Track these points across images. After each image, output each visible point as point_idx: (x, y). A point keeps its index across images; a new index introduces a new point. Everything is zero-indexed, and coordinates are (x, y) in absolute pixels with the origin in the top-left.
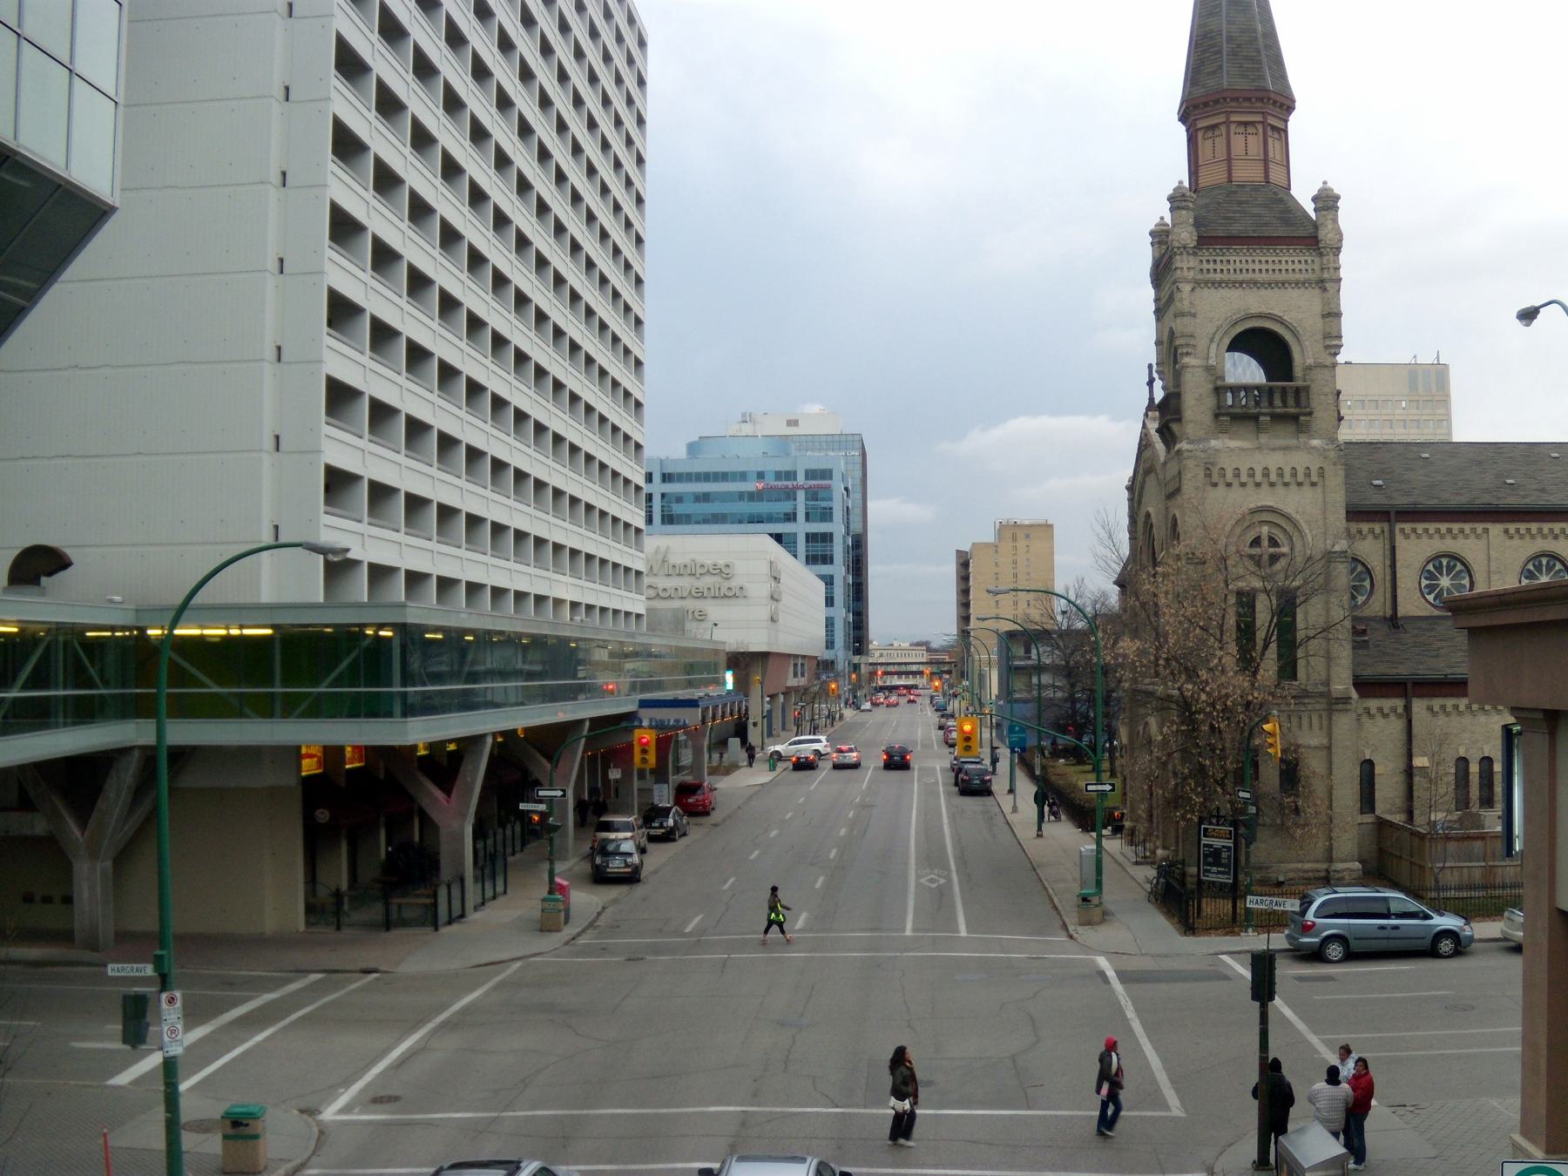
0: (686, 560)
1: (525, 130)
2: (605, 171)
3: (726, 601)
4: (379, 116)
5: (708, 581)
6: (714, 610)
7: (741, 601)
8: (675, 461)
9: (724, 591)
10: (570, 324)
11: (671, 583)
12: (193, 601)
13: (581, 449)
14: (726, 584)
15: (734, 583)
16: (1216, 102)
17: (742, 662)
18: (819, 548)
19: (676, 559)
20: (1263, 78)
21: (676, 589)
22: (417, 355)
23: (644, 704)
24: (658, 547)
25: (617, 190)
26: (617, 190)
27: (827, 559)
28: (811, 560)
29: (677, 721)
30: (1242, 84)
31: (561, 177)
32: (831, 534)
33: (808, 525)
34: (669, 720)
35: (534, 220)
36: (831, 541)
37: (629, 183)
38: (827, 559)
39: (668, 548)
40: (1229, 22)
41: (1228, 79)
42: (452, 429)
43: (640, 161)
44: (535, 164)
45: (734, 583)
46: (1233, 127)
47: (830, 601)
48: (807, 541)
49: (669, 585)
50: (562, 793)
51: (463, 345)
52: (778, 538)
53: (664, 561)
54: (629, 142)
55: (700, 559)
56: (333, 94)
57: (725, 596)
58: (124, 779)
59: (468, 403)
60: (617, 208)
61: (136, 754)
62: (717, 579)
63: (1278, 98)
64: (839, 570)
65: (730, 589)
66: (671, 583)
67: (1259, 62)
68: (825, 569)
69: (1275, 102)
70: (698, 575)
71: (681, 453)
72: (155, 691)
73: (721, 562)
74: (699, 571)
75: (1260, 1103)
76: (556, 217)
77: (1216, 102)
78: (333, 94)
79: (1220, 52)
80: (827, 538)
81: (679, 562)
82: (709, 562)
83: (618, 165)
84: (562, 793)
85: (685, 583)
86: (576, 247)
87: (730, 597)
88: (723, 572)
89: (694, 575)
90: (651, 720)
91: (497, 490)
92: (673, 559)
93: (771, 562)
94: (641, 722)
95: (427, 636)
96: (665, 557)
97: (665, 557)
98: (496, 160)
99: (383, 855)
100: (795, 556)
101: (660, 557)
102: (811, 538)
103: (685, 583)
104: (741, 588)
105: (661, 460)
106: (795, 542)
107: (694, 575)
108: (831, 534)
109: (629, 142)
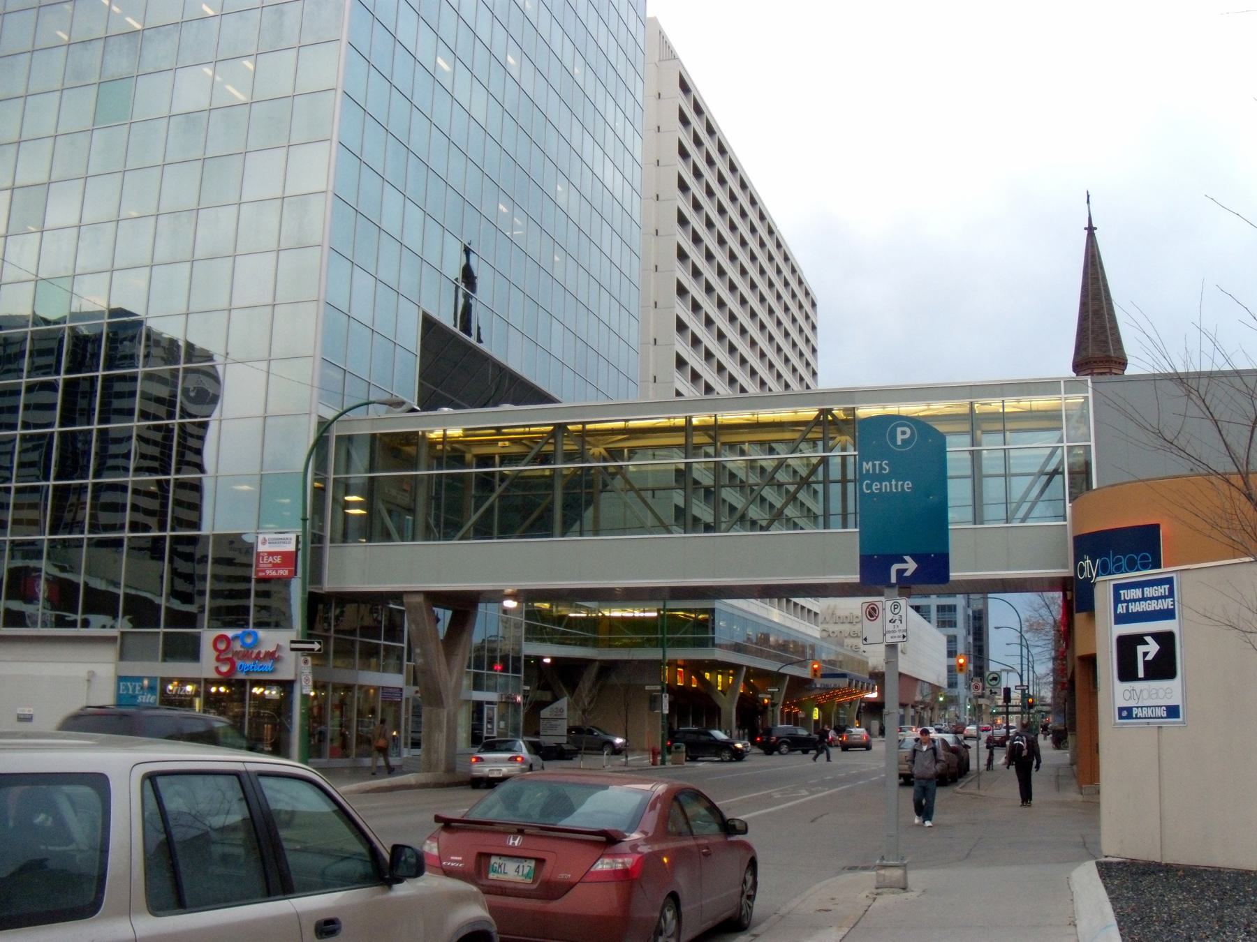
0: (847, 613)
1: (743, 301)
2: (794, 334)
16: (1086, 363)
18: (947, 616)
20: (1109, 350)
25: (801, 344)
26: (801, 344)
27: (953, 624)
28: (942, 624)
29: (835, 685)
30: (1098, 354)
31: (771, 338)
32: (955, 606)
33: (955, 633)
35: (749, 349)
36: (955, 610)
37: (808, 340)
38: (953, 624)
39: (835, 606)
40: (1093, 324)
41: (1092, 351)
43: (814, 327)
44: (739, 306)
46: (1008, 434)
47: (952, 654)
48: (938, 611)
52: (917, 609)
54: (807, 317)
56: (677, 305)
58: (591, 674)
60: (801, 355)
61: (597, 663)
63: (1119, 361)
64: (960, 631)
67: (1107, 343)
68: (951, 631)
69: (1115, 362)
74: (855, 620)
76: (730, 310)
77: (1086, 363)
78: (677, 305)
79: (1088, 339)
80: (952, 608)
83: (801, 331)
86: (771, 366)
92: (839, 613)
98: (706, 289)
100: (929, 622)
101: (830, 612)
102: (941, 609)
106: (929, 612)
108: (955, 606)
109: (807, 317)
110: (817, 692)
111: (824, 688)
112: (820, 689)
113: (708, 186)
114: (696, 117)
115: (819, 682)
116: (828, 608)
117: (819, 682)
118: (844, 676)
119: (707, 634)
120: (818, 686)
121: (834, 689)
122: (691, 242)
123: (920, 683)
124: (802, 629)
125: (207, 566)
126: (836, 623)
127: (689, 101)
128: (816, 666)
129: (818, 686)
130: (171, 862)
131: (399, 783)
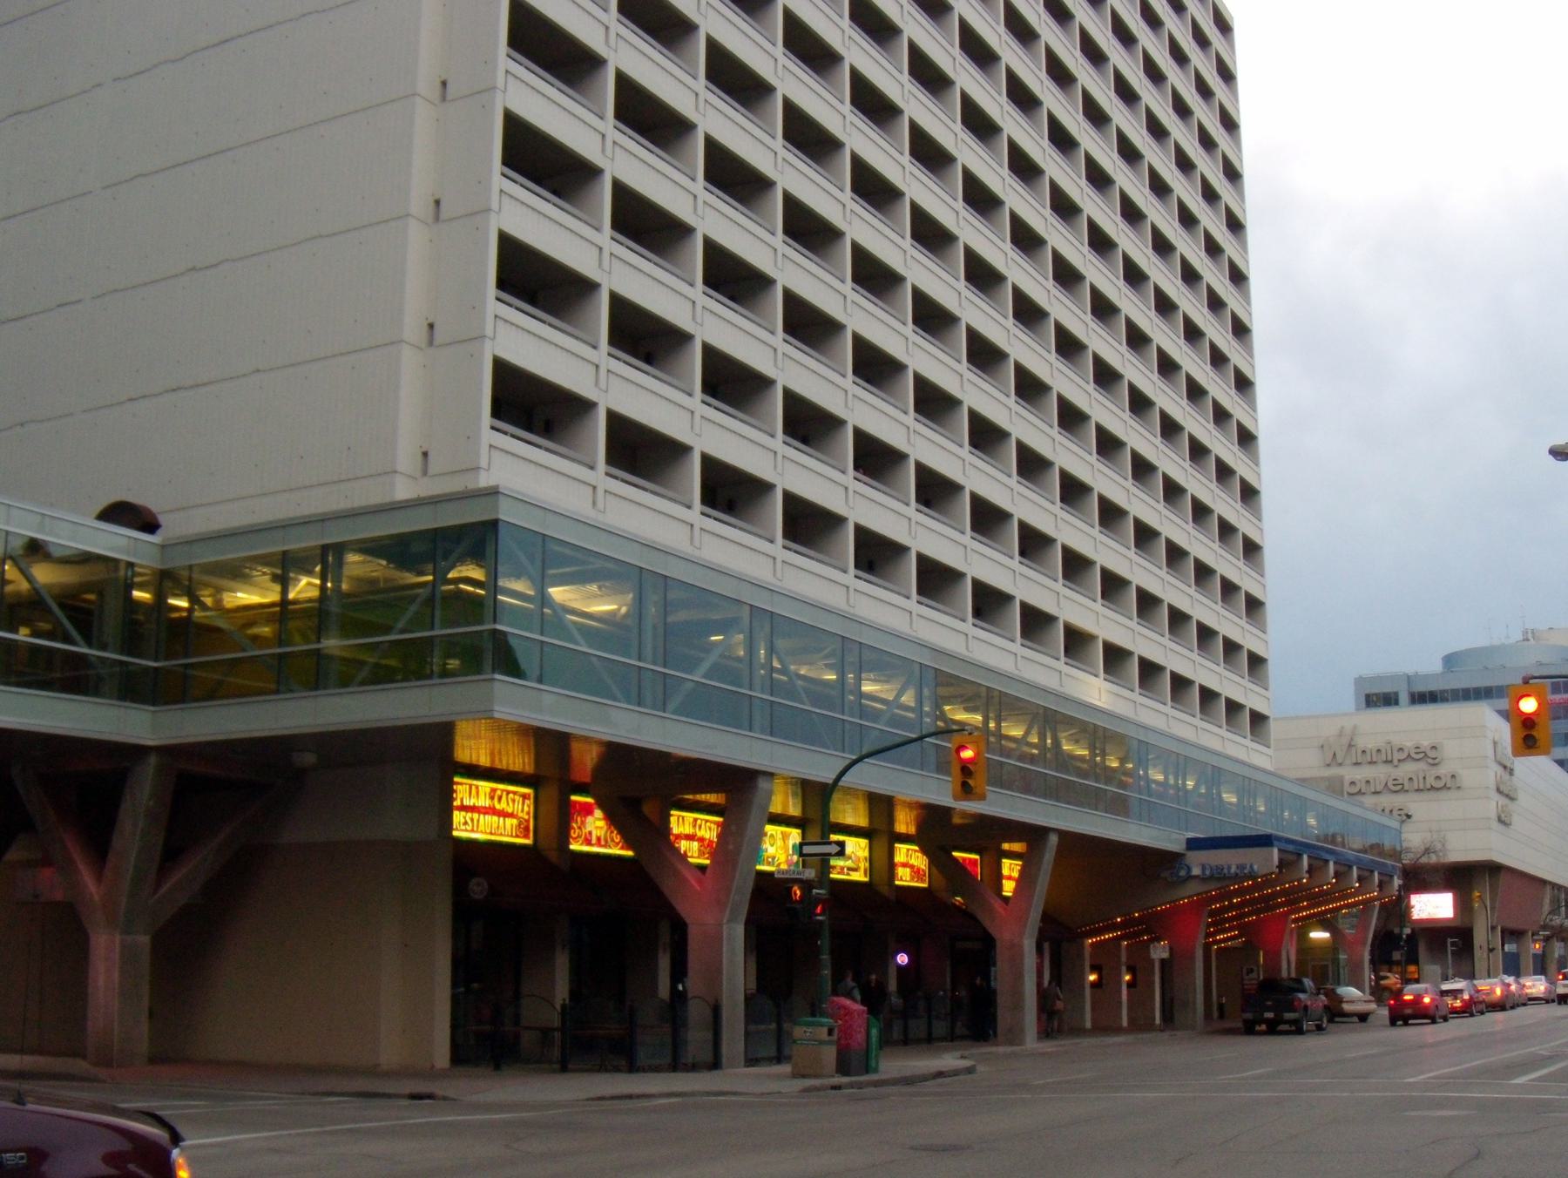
3: (1433, 795)
4: (1094, 319)
5: (1409, 768)
6: (1419, 806)
7: (1452, 794)
8: (1426, 677)
9: (1431, 781)
10: (1239, 462)
11: (1360, 774)
12: (840, 783)
13: (1215, 571)
14: (1434, 772)
15: (1443, 770)
17: (1458, 877)
19: (1368, 742)
21: (1368, 782)
22: (1178, 618)
23: (1193, 844)
24: (1342, 728)
29: (1241, 867)
34: (1229, 868)
39: (1355, 727)
42: (1185, 671)
45: (1443, 770)
49: (1358, 777)
50: (839, 849)
51: (1243, 622)
53: (1350, 746)
55: (1397, 741)
57: (1432, 788)
59: (1200, 646)
61: (153, 760)
62: (1422, 765)
65: (1438, 778)
66: (1360, 774)
70: (1395, 762)
71: (1437, 667)
72: (1158, 1021)
73: (1425, 743)
74: (1397, 756)
75: (1413, 894)
81: (1370, 746)
82: (1409, 744)
84: (839, 849)
85: (1380, 773)
87: (1438, 789)
88: (1428, 755)
89: (1391, 762)
90: (1204, 868)
91: (1206, 718)
92: (1361, 742)
93: (1495, 743)
94: (1189, 869)
95: (721, 637)
96: (1352, 739)
97: (1352, 739)
99: (858, 1007)
101: (1345, 741)
103: (1380, 773)
104: (1453, 776)
105: (1409, 677)
107: (1391, 762)
110: (1193, 888)
111: (1211, 878)
112: (1202, 879)
113: (1202, 130)
114: (1197, 49)
115: (1197, 863)
116: (1340, 735)
117: (1197, 863)
118: (1264, 841)
119: (481, 622)
120: (1196, 871)
121: (1237, 878)
122: (1227, 282)
123: (1548, 888)
124: (1241, 754)
125: (117, 654)
126: (1357, 764)
127: (1185, 25)
128: (968, 754)
129: (1196, 871)
130: (1355, 1019)
131: (97, 1120)
